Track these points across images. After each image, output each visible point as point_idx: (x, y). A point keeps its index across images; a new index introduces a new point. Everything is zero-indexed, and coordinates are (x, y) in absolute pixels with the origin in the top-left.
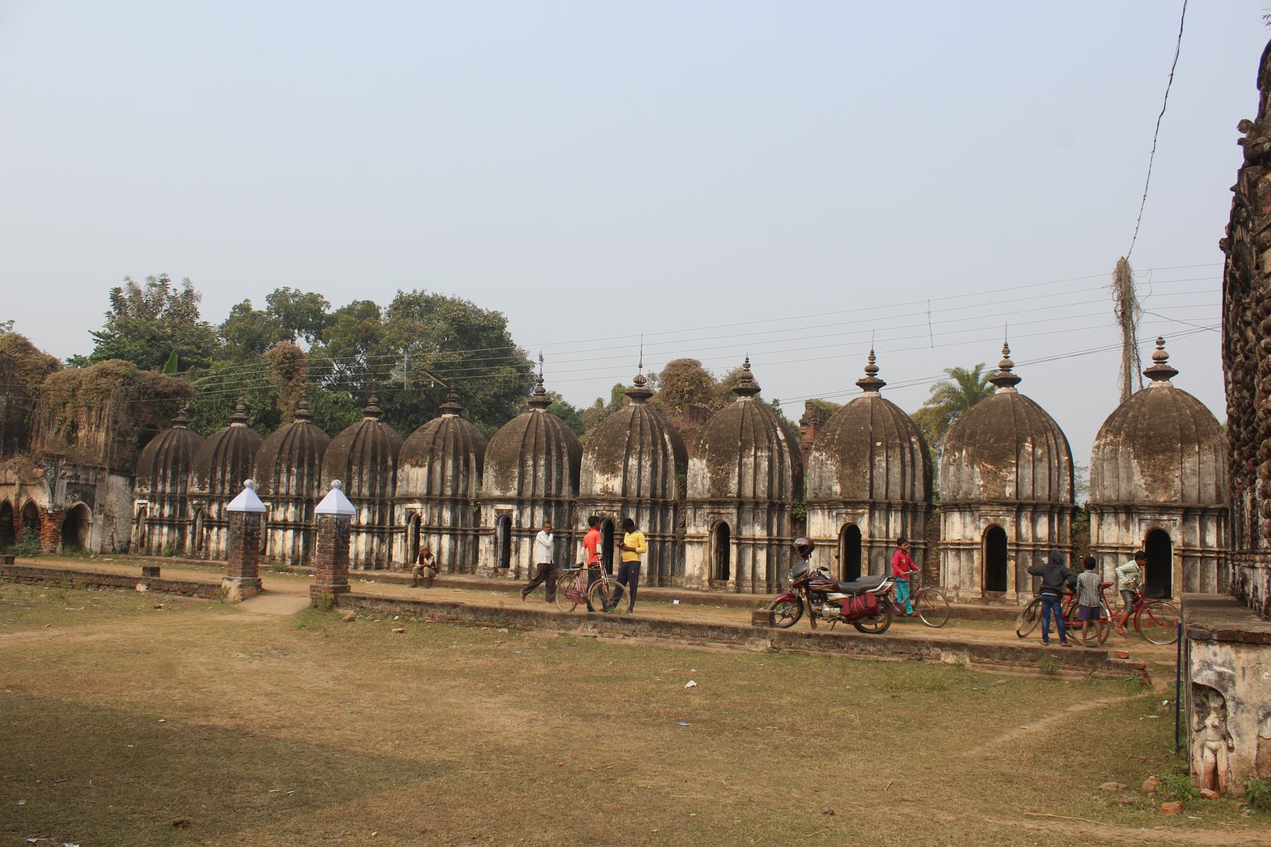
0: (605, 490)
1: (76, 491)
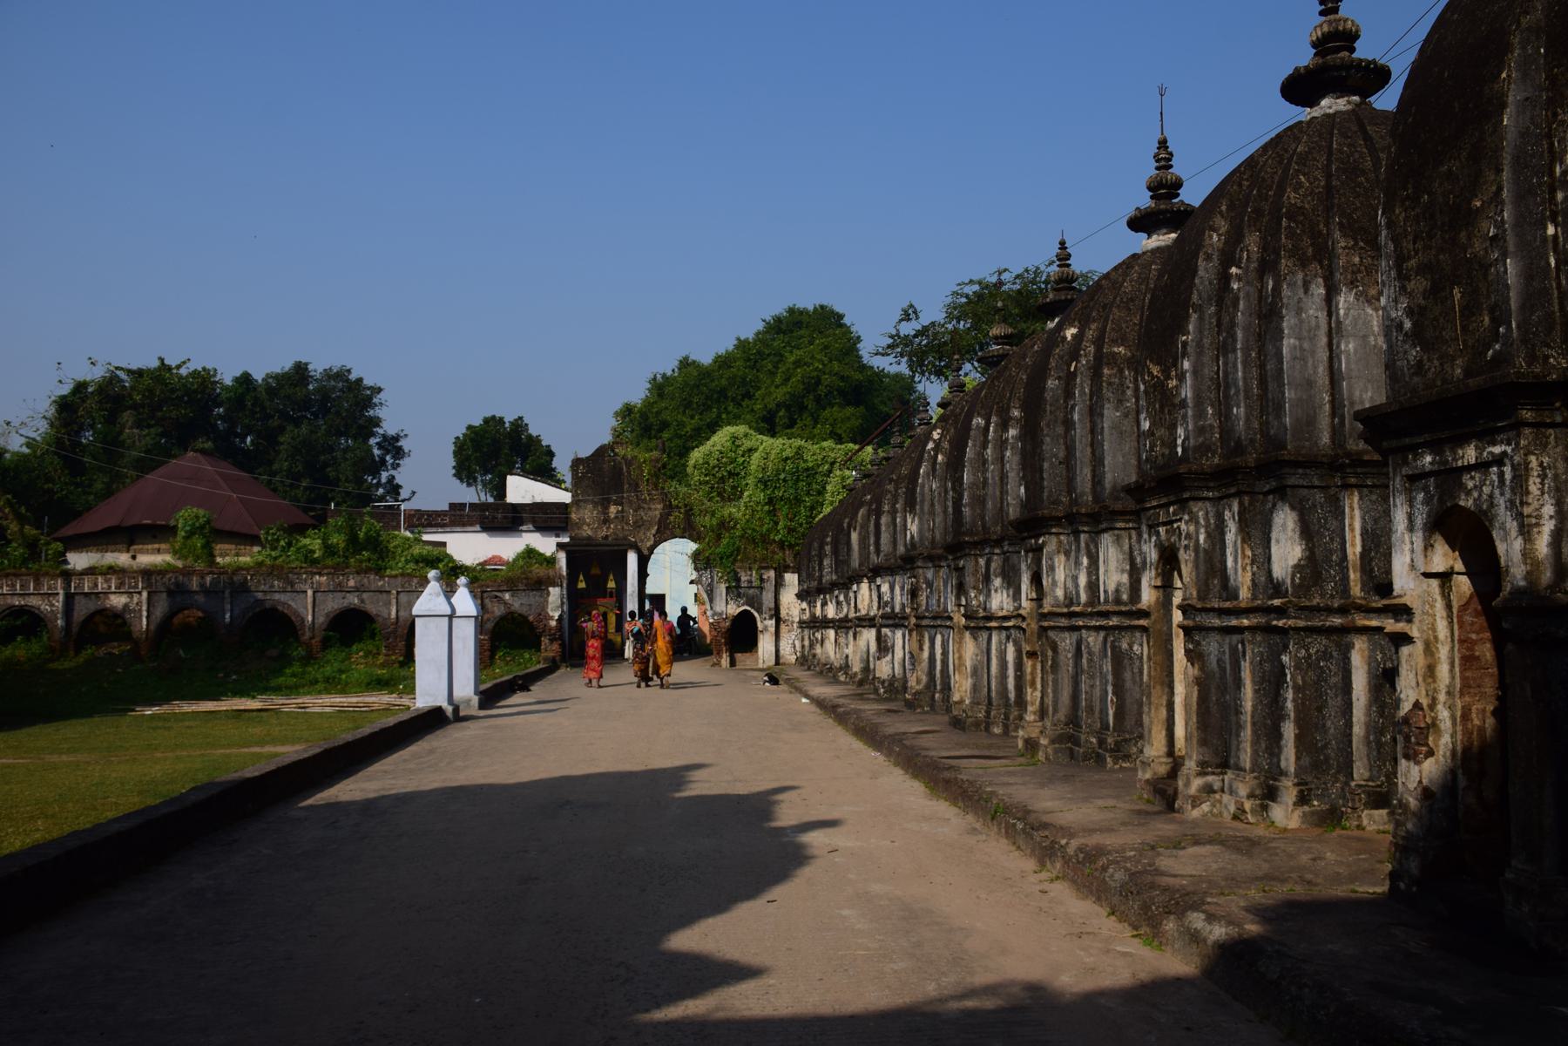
1: (739, 595)
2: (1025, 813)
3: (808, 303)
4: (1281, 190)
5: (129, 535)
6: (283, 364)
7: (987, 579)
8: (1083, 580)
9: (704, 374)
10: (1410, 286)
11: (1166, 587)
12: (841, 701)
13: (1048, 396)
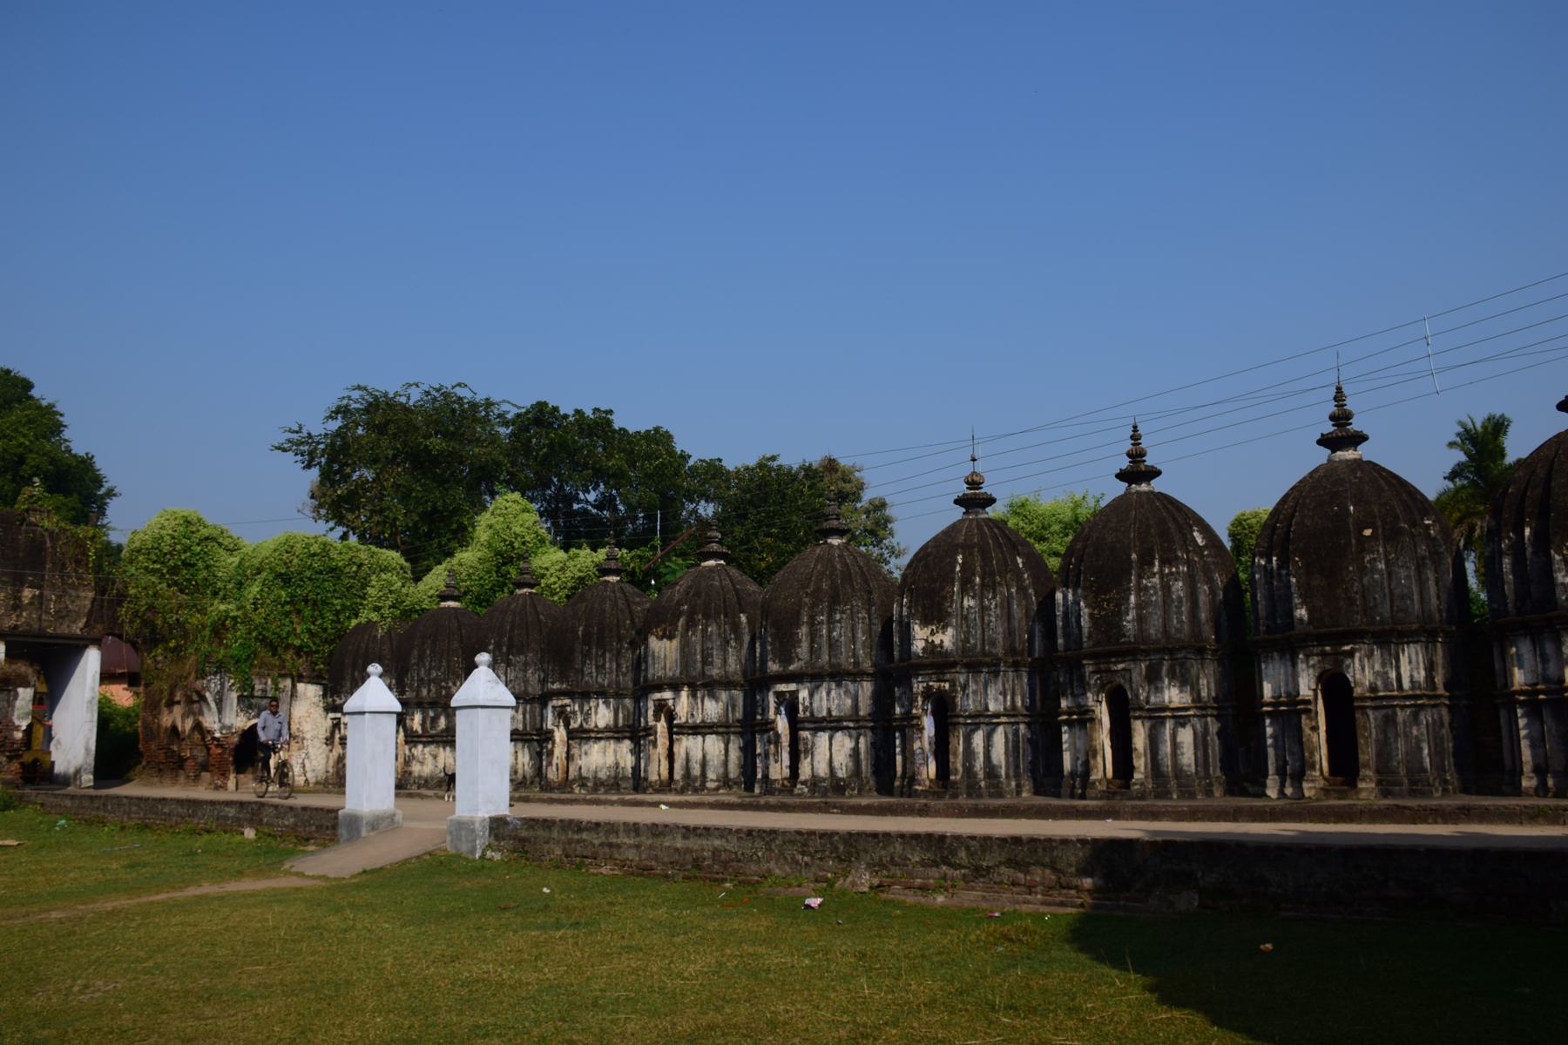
0: (931, 648)
9: (786, 478)
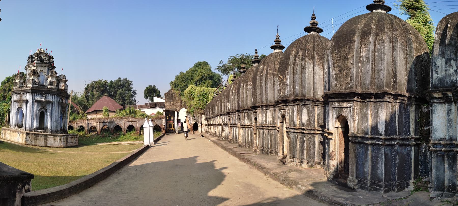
2: (261, 166)
3: (201, 61)
4: (306, 45)
5: (96, 112)
6: (117, 78)
7: (244, 117)
8: (264, 119)
9: (185, 75)
10: (335, 69)
11: (282, 123)
12: (217, 141)
13: (257, 80)
